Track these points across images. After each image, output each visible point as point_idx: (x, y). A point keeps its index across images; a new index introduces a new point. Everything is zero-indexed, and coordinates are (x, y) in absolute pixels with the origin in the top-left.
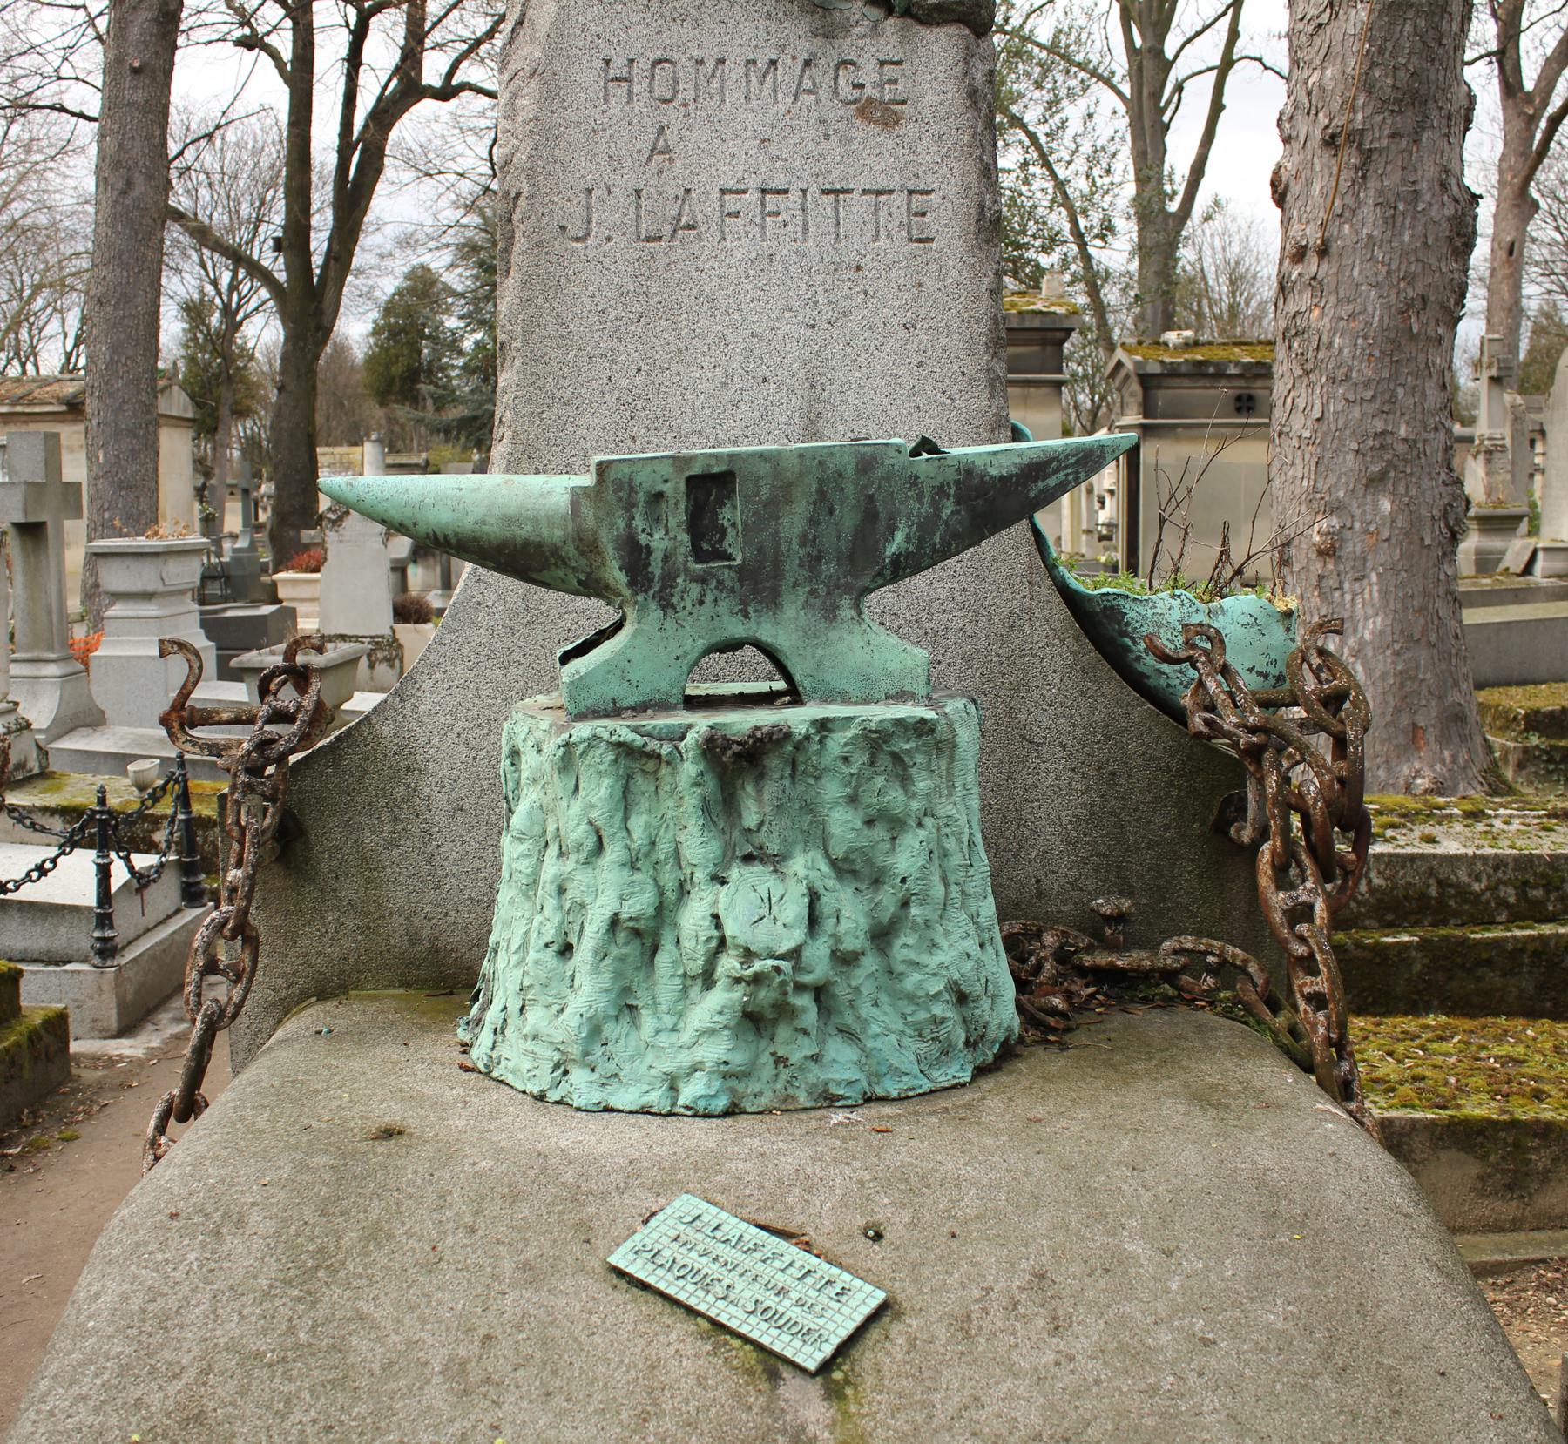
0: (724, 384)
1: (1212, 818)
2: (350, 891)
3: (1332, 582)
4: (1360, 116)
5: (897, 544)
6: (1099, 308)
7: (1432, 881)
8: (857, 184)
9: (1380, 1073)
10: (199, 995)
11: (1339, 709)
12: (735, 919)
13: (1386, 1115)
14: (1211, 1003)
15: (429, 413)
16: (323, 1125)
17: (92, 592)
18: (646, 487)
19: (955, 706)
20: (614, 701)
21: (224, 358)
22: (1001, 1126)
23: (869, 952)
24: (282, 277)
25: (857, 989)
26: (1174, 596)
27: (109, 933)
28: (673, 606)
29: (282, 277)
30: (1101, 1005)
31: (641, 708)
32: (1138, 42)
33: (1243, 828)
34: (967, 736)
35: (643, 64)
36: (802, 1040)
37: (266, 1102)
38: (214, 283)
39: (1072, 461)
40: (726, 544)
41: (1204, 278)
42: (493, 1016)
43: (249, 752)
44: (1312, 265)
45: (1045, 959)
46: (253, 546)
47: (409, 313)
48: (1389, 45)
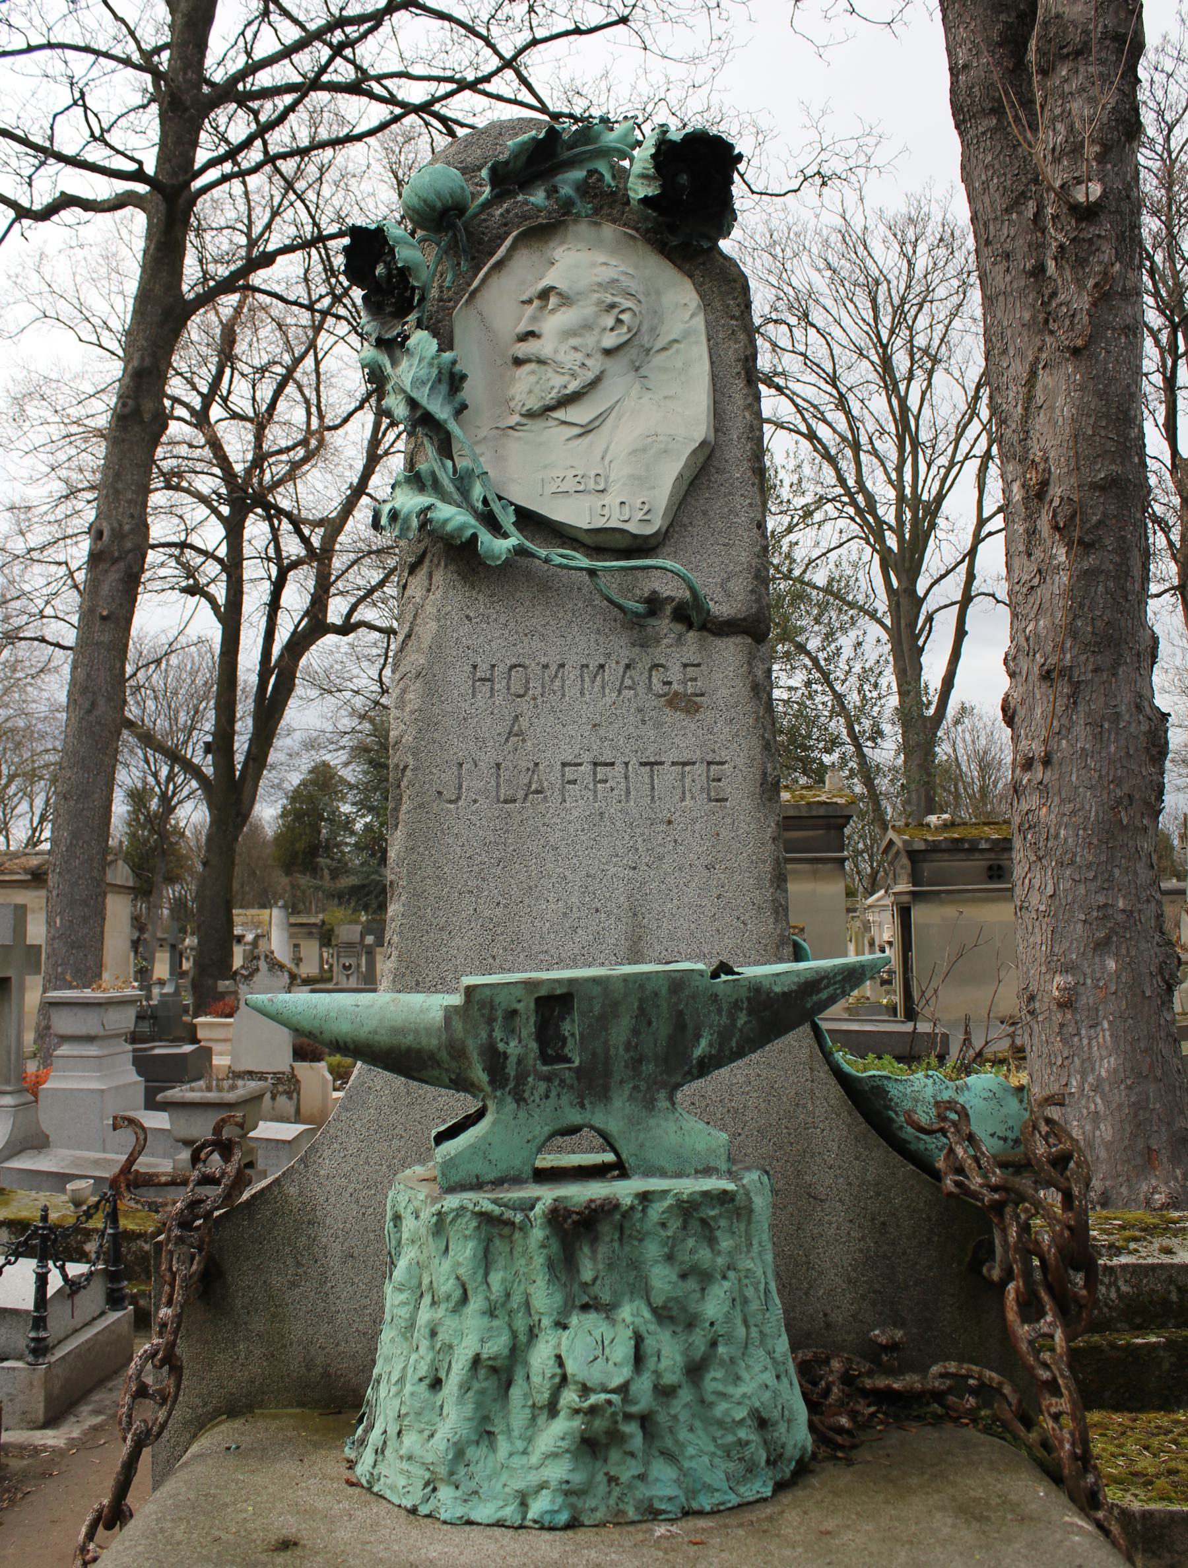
0: (565, 914)
1: (967, 1259)
2: (258, 1324)
3: (1072, 1029)
4: (1068, 656)
5: (702, 1048)
6: (874, 795)
7: (1172, 1288)
8: (668, 758)
9: (1139, 1467)
10: (130, 1416)
11: (1065, 1167)
12: (575, 1359)
13: (1147, 1507)
14: (974, 1421)
15: (327, 883)
16: (231, 1537)
17: (44, 1032)
18: (503, 1005)
19: (751, 1178)
20: (477, 1177)
21: (160, 835)
22: (798, 1538)
23: (684, 1385)
24: (209, 771)
25: (675, 1418)
26: (927, 1076)
27: (43, 1334)
28: (525, 1100)
29: (209, 771)
30: (881, 1423)
31: (499, 1183)
32: (895, 584)
33: (993, 1268)
34: (761, 1203)
35: (502, 668)
36: (630, 1462)
37: (183, 1514)
38: (155, 775)
39: (839, 978)
40: (566, 1050)
41: (959, 765)
42: (375, 1437)
43: (182, 1210)
44: (1039, 773)
45: (833, 1383)
46: (177, 992)
47: (311, 799)
48: (1087, 602)
